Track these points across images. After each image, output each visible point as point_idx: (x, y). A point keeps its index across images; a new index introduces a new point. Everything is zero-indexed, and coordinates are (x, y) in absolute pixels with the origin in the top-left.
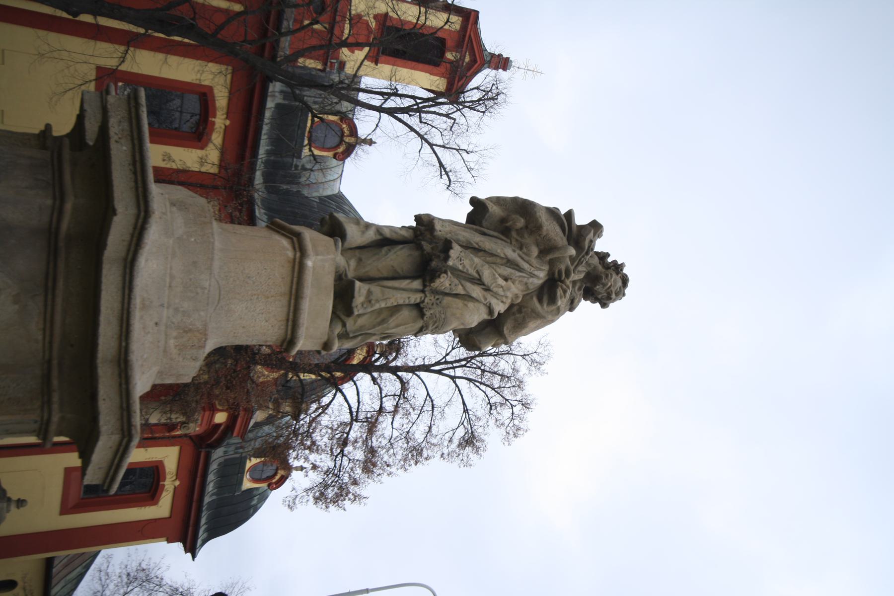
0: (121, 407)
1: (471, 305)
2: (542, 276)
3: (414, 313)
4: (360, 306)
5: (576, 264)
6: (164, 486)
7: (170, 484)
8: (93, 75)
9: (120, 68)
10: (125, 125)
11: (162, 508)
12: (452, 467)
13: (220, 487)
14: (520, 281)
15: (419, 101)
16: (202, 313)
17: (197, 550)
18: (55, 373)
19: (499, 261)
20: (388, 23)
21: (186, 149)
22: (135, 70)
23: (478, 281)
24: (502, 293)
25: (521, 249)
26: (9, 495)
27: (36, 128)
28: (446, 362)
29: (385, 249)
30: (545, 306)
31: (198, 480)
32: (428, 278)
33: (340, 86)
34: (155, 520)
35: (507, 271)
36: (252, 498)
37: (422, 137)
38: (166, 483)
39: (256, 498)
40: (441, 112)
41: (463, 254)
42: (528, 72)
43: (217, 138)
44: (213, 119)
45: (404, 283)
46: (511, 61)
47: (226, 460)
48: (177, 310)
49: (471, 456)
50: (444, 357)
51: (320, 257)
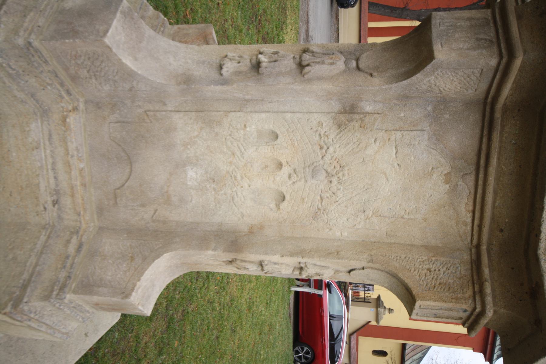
17: (494, 361)
18: (485, 259)
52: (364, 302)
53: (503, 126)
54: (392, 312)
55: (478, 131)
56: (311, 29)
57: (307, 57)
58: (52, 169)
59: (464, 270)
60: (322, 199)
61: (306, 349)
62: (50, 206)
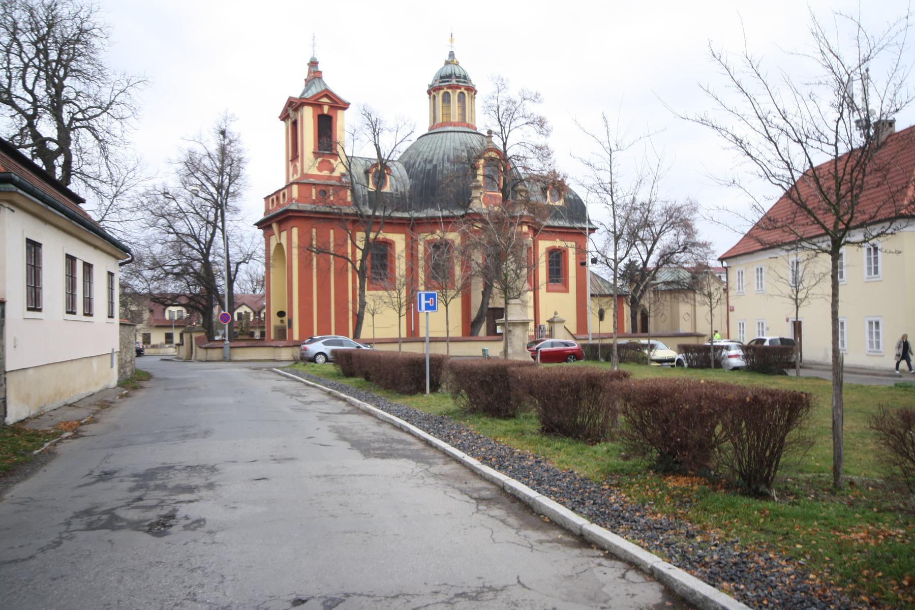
7: (558, 243)
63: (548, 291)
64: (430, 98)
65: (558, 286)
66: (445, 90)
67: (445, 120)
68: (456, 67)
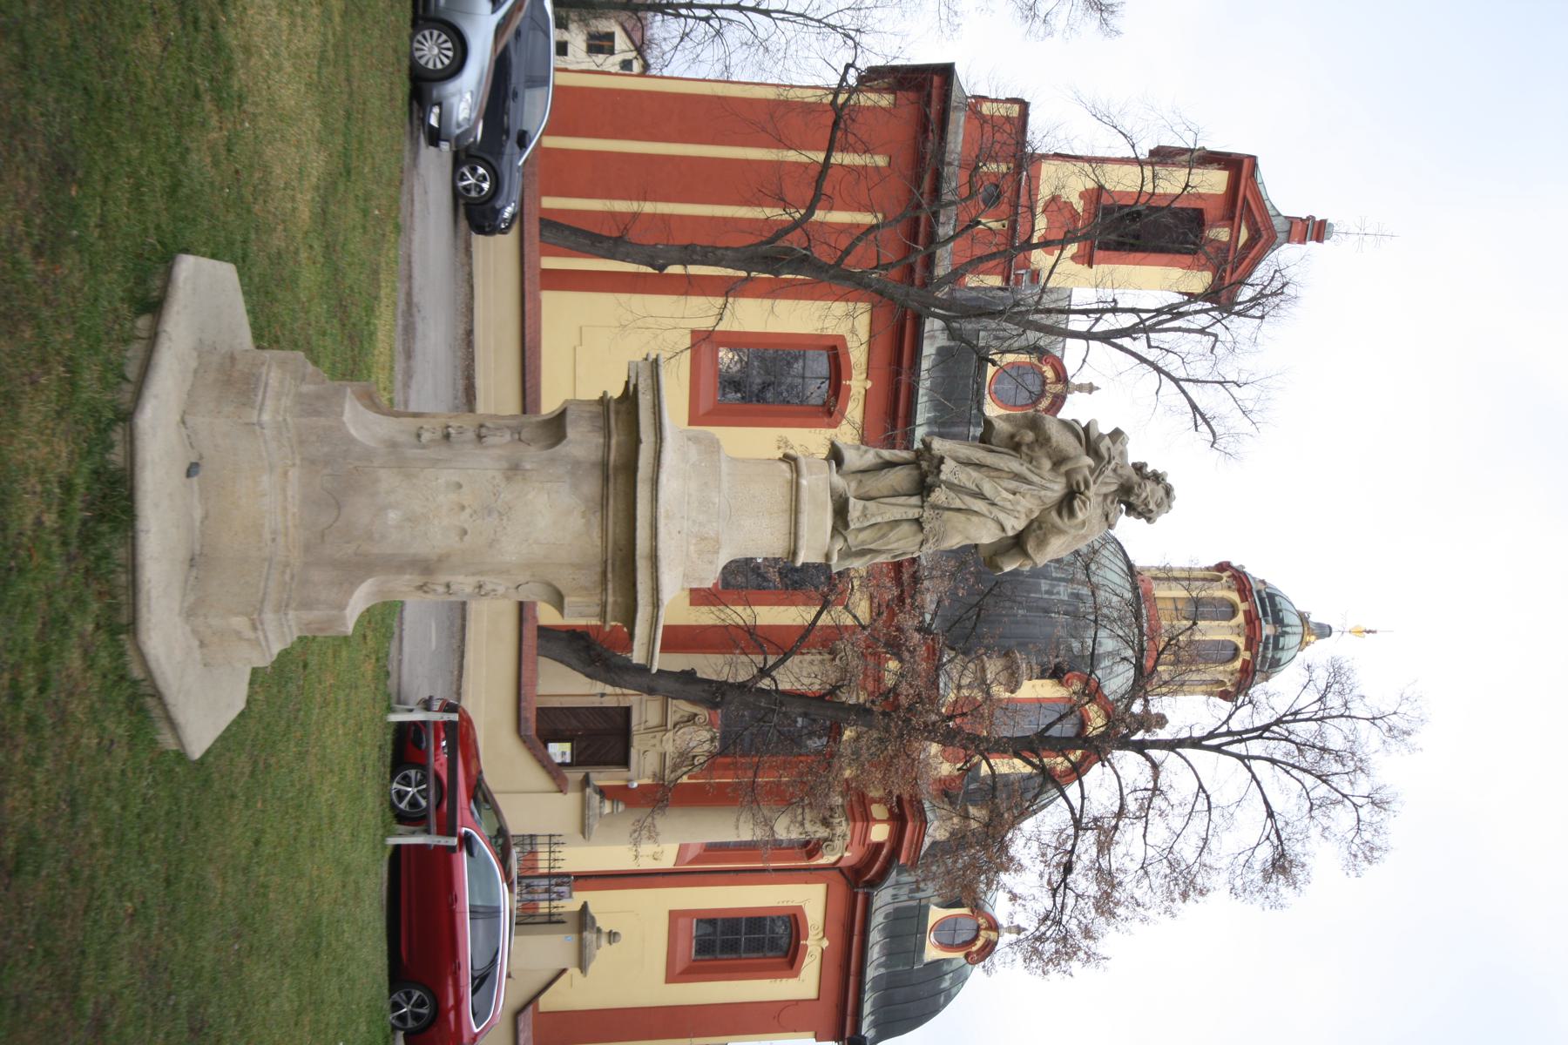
0: (653, 588)
1: (975, 519)
2: (1057, 488)
3: (915, 527)
4: (855, 520)
5: (1096, 474)
6: (806, 947)
7: (815, 944)
8: (687, 342)
9: (717, 329)
10: (649, 381)
11: (804, 984)
12: (1251, 911)
13: (890, 953)
14: (1032, 495)
15: (1144, 316)
16: (714, 524)
18: (610, 568)
19: (1004, 475)
20: (1105, 200)
21: (813, 430)
22: (736, 328)
23: (980, 495)
24: (1010, 507)
25: (1031, 462)
26: (599, 924)
27: (596, 396)
28: (1229, 733)
29: (886, 470)
30: (1066, 519)
31: (856, 939)
32: (925, 494)
33: (1016, 310)
34: (797, 1002)
35: (1013, 485)
36: (941, 977)
37: (1159, 370)
38: (808, 943)
39: (947, 977)
40: (1193, 326)
41: (958, 469)
42: (1366, 238)
43: (854, 410)
44: (848, 382)
45: (902, 500)
46: (1331, 225)
47: (896, 910)
48: (694, 521)
49: (1283, 890)
50: (1226, 722)
51: (814, 477)
52: (550, 922)
53: (615, 479)
54: (617, 938)
55: (600, 482)
56: (416, 290)
57: (484, 431)
58: (830, 414)
59: (597, 577)
60: (495, 532)
61: (416, 994)
62: (269, 543)
63: (674, 916)
64: (1208, 569)
65: (687, 949)
66: (1242, 607)
67: (1160, 605)
68: (1297, 639)
